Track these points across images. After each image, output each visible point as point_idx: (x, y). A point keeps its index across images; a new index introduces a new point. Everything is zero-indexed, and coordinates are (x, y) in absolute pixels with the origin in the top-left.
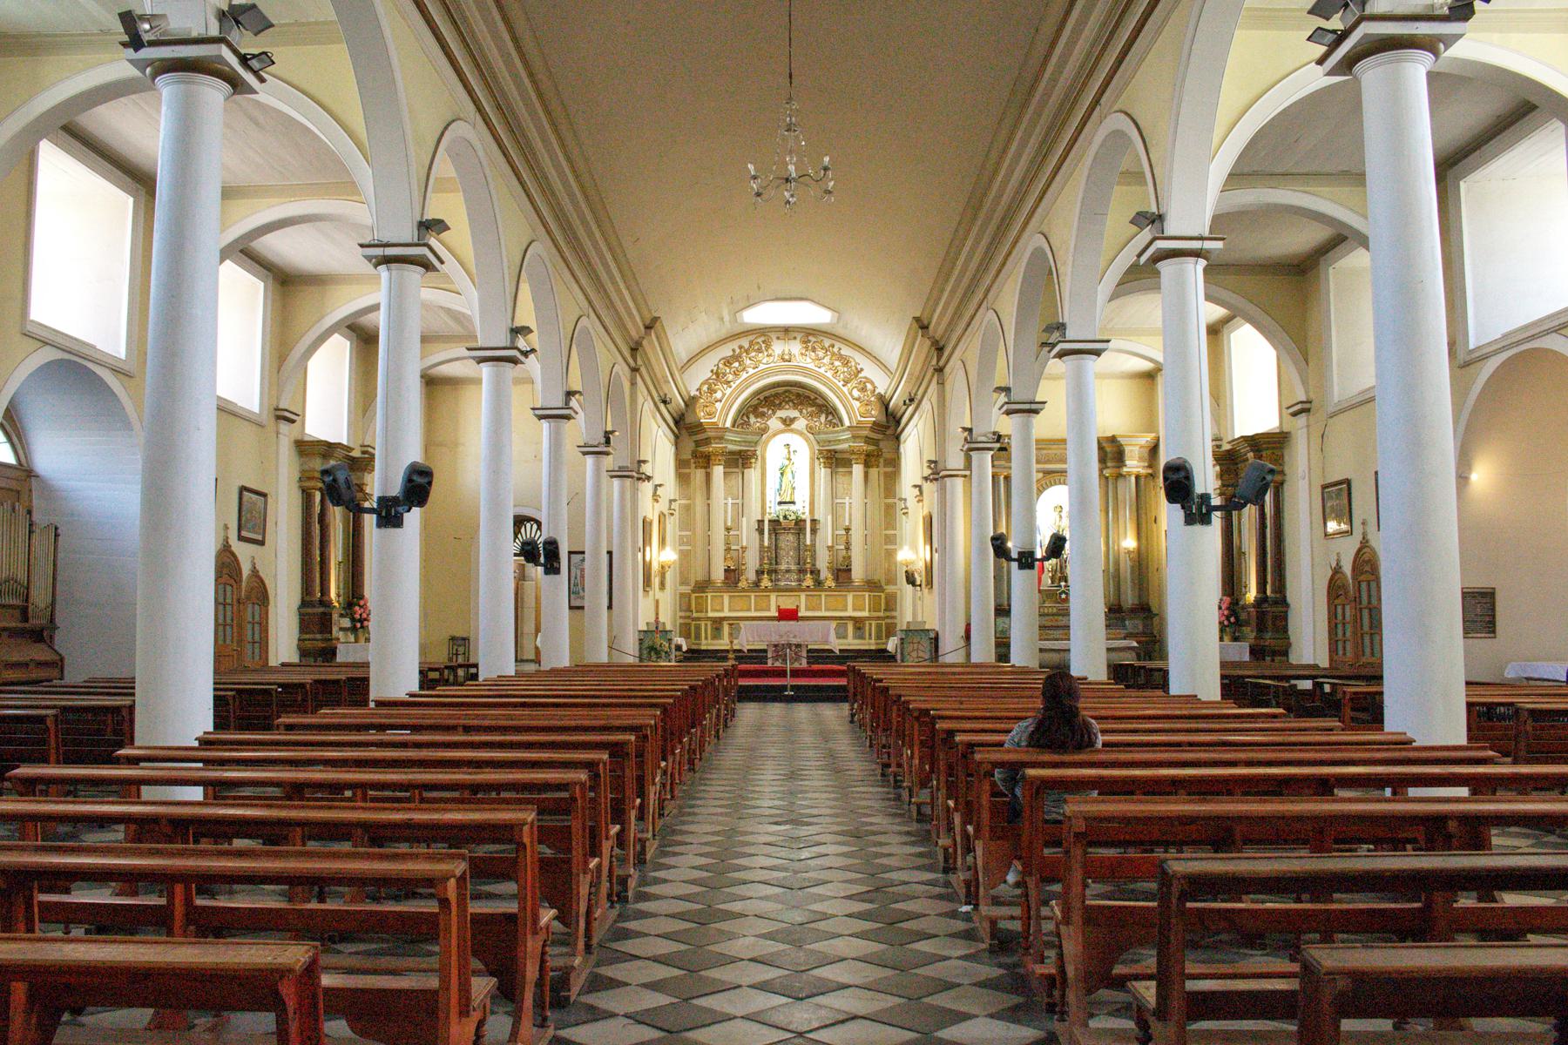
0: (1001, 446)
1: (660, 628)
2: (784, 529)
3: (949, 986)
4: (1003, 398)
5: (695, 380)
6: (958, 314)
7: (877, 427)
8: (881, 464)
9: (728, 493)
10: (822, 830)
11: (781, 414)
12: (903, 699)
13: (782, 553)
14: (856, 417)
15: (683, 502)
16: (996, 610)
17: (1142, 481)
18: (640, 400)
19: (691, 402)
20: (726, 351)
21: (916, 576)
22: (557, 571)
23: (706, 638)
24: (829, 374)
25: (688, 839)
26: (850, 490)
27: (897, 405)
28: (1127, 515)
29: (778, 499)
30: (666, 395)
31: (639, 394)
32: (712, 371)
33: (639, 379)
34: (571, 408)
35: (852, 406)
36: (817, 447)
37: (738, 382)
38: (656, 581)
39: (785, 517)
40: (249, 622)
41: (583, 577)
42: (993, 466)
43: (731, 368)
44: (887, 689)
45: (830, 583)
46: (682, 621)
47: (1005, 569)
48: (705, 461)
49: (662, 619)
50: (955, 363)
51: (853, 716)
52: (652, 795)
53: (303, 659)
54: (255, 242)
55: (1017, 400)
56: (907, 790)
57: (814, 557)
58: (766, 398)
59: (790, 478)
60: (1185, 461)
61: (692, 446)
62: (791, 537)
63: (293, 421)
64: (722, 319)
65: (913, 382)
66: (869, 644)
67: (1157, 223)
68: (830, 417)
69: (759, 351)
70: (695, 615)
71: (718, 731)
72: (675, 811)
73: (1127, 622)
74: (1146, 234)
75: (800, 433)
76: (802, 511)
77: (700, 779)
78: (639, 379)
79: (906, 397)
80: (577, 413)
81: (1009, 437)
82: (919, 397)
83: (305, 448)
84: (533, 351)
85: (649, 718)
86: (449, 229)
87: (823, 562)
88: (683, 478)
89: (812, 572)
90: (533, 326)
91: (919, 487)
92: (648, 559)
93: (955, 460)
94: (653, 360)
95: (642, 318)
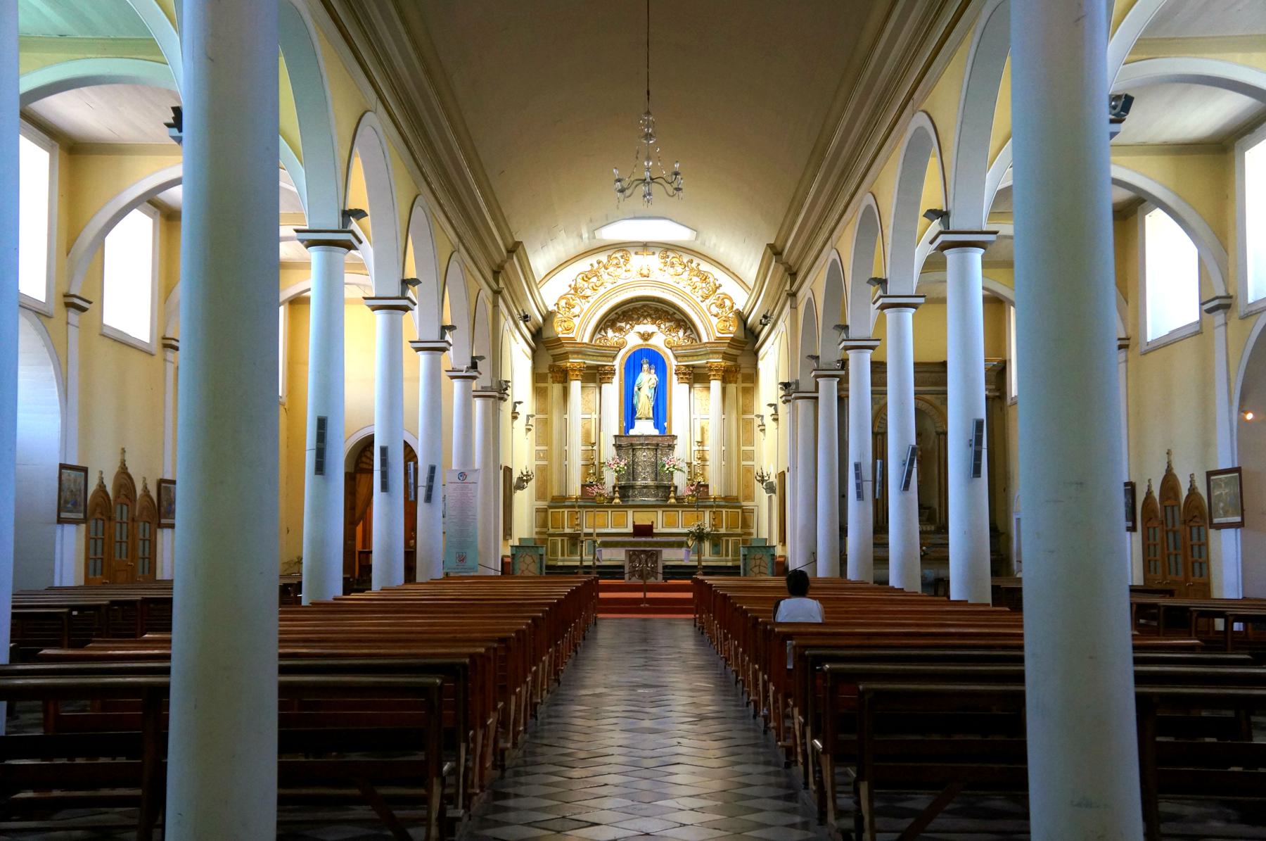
4: (936, 226)
7: (734, 342)
8: (740, 379)
15: (541, 416)
19: (548, 317)
23: (563, 554)
32: (570, 286)
33: (500, 301)
40: (141, 539)
48: (563, 376)
54: (161, 194)
55: (854, 337)
58: (624, 313)
61: (549, 361)
63: (83, 310)
66: (727, 561)
70: (551, 531)
78: (500, 301)
80: (360, 242)
82: (775, 316)
88: (540, 391)
90: (368, 211)
95: (505, 245)
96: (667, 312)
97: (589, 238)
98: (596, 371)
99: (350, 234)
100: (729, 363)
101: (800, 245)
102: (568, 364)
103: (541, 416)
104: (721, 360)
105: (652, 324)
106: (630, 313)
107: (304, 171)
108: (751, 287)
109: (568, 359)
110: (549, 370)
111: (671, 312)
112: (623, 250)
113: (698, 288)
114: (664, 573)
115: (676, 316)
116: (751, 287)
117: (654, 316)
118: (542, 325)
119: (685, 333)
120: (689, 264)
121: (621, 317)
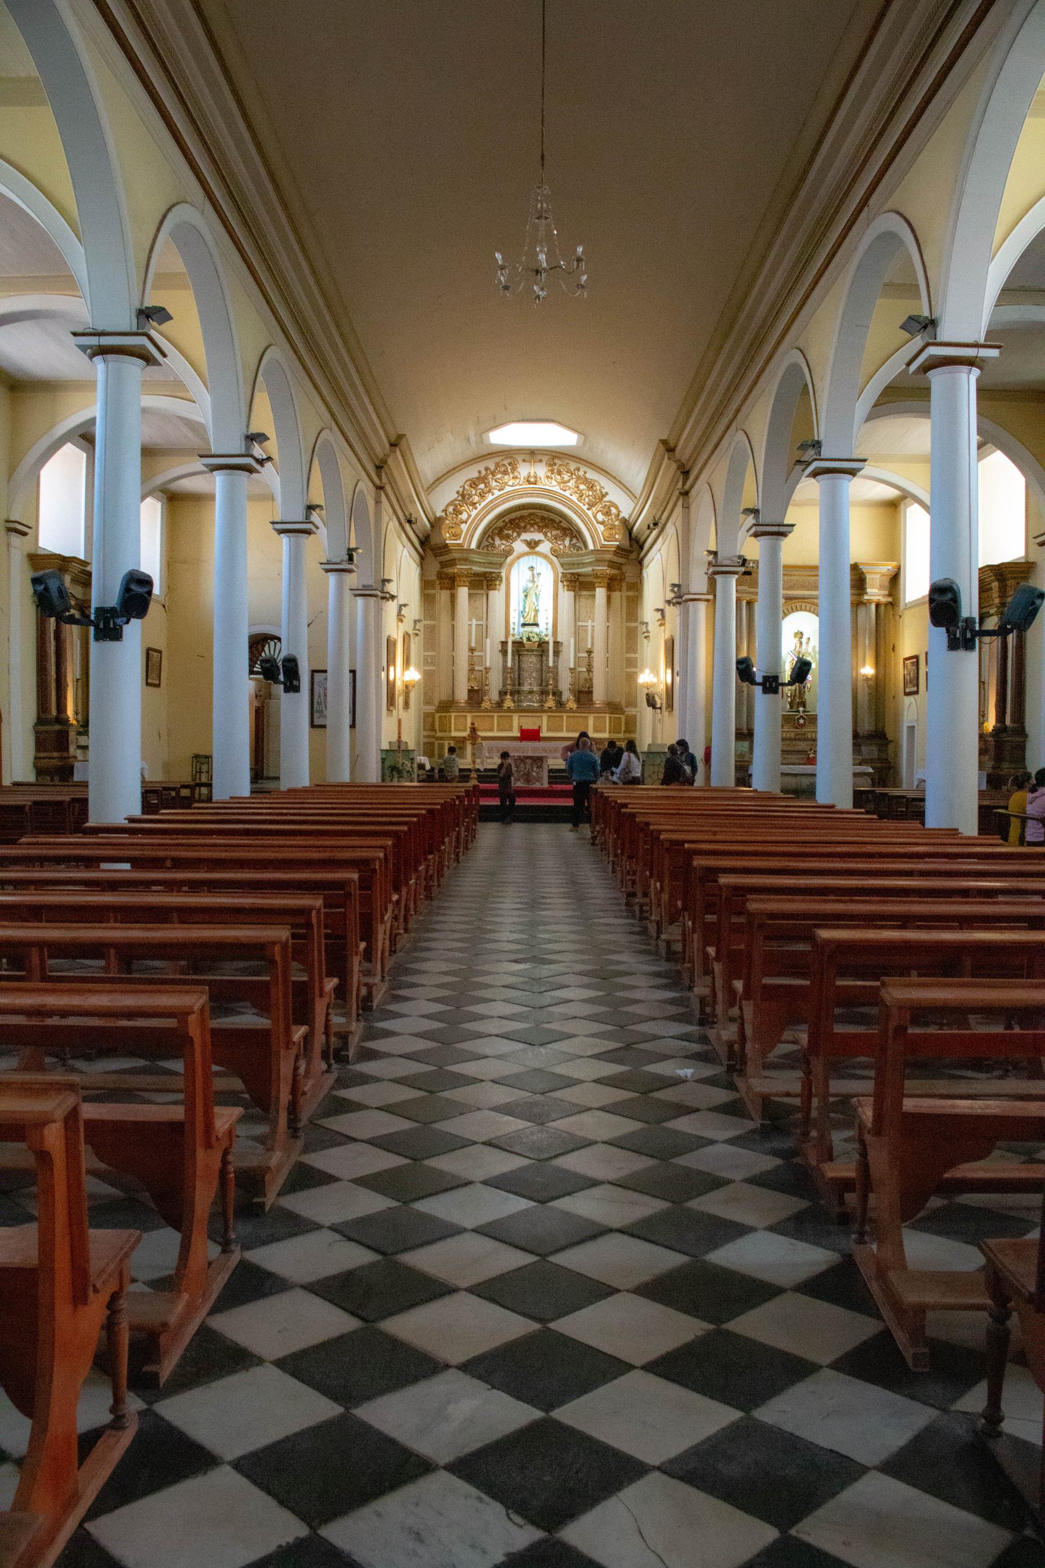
0: (746, 571)
1: (403, 748)
2: (528, 651)
3: (689, 1111)
4: (750, 520)
5: (442, 500)
6: (706, 436)
7: (620, 550)
8: (624, 588)
10: (567, 970)
11: (527, 536)
12: (652, 827)
13: (525, 674)
14: (600, 540)
15: (429, 622)
16: (737, 734)
17: (882, 608)
19: (436, 523)
20: (472, 473)
21: (657, 699)
22: (296, 689)
24: (574, 498)
25: (432, 945)
26: (593, 613)
28: (867, 642)
29: (522, 621)
30: (411, 514)
31: (384, 513)
35: (596, 530)
37: (483, 504)
38: (400, 700)
39: (529, 639)
41: (325, 695)
42: (737, 591)
44: (633, 815)
45: (572, 705)
46: (426, 740)
47: (745, 692)
48: (450, 582)
49: (404, 739)
51: (594, 838)
52: (380, 936)
53: (40, 779)
55: (768, 521)
56: (654, 924)
58: (511, 521)
59: (534, 600)
60: (953, 582)
62: (533, 659)
63: (24, 534)
67: (929, 328)
68: (574, 541)
69: (505, 473)
70: (439, 734)
71: (457, 855)
72: (408, 945)
73: (863, 748)
74: (918, 341)
75: (545, 556)
76: (545, 632)
77: (439, 907)
79: (651, 522)
80: (317, 528)
81: (756, 562)
82: (663, 521)
83: (37, 559)
84: (269, 459)
85: (376, 850)
86: (172, 318)
87: (565, 683)
89: (554, 694)
91: (662, 611)
92: (391, 678)
93: (699, 584)
94: (400, 483)
96: (553, 521)
99: (145, 338)
101: (694, 440)
102: (456, 571)
103: (429, 622)
105: (539, 532)
106: (517, 521)
107: (83, 251)
108: (638, 493)
111: (557, 521)
114: (550, 777)
116: (638, 493)
118: (430, 532)
119: (571, 541)
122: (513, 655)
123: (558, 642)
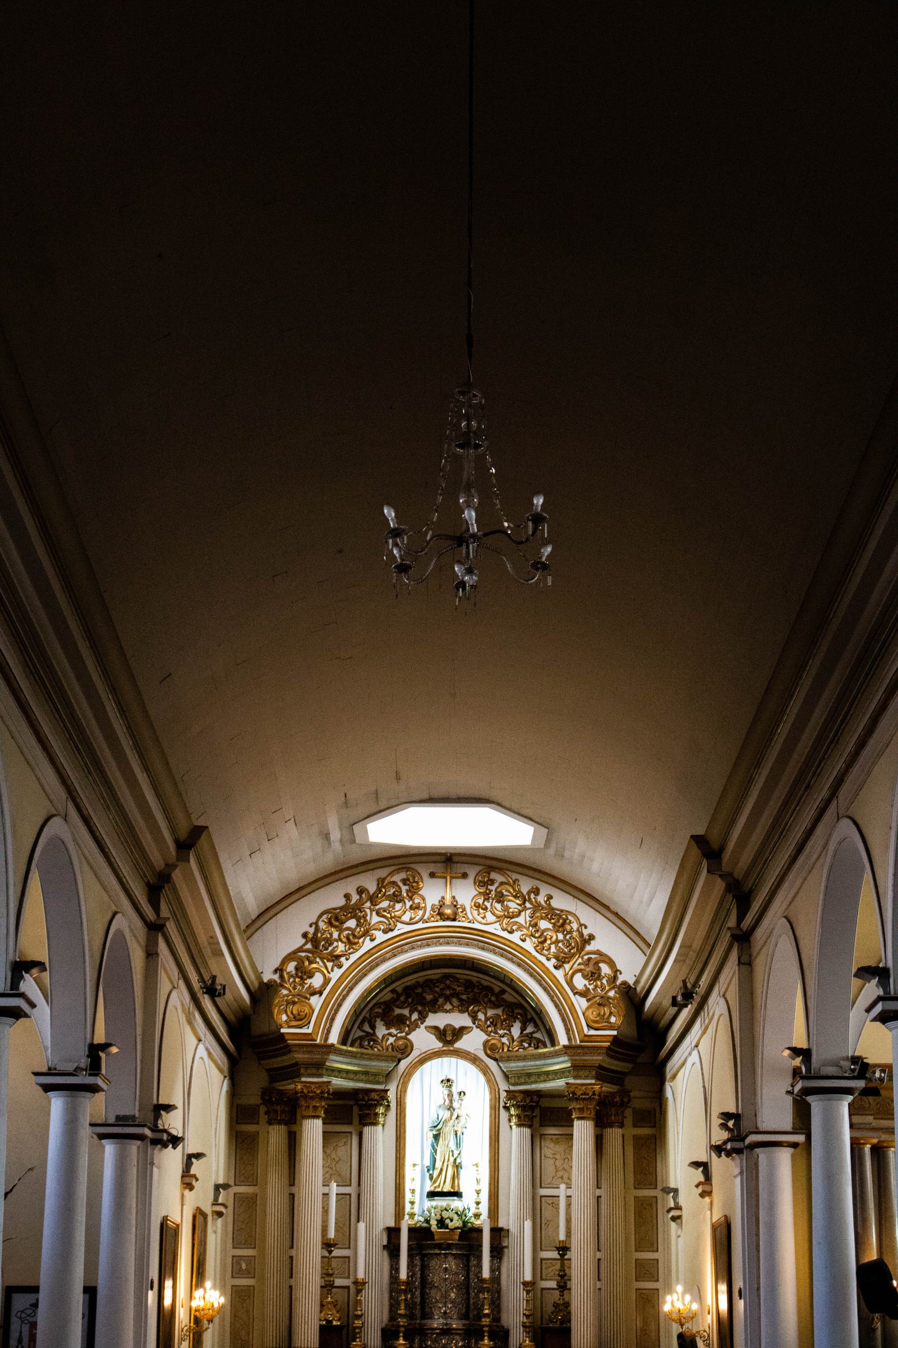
2: (440, 1246)
4: (872, 989)
8: (629, 1121)
9: (331, 1173)
13: (435, 1295)
14: (580, 1030)
18: (164, 986)
24: (529, 945)
27: (657, 1005)
29: (429, 1187)
30: (214, 978)
32: (305, 935)
34: (22, 995)
35: (572, 1007)
36: (503, 1086)
37: (354, 957)
39: (441, 1223)
43: (341, 931)
50: (774, 919)
57: (496, 1305)
58: (408, 990)
59: (452, 1146)
62: (451, 1264)
64: (327, 836)
65: (689, 962)
68: (530, 1029)
69: (396, 898)
75: (473, 1059)
76: (473, 1210)
79: (676, 989)
80: (33, 1005)
81: (887, 1069)
91: (704, 1167)
92: (167, 1302)
94: (191, 910)
95: (173, 830)
96: (489, 989)
97: (341, 841)
98: (352, 1103)
100: (607, 1088)
104: (593, 1081)
105: (461, 1012)
106: (420, 990)
109: (299, 1076)
110: (262, 1098)
111: (497, 990)
112: (408, 869)
113: (549, 942)
115: (506, 996)
117: (464, 997)
118: (250, 1011)
119: (523, 1029)
120: (532, 896)
121: (402, 999)
122: (410, 1256)
123: (502, 1229)
